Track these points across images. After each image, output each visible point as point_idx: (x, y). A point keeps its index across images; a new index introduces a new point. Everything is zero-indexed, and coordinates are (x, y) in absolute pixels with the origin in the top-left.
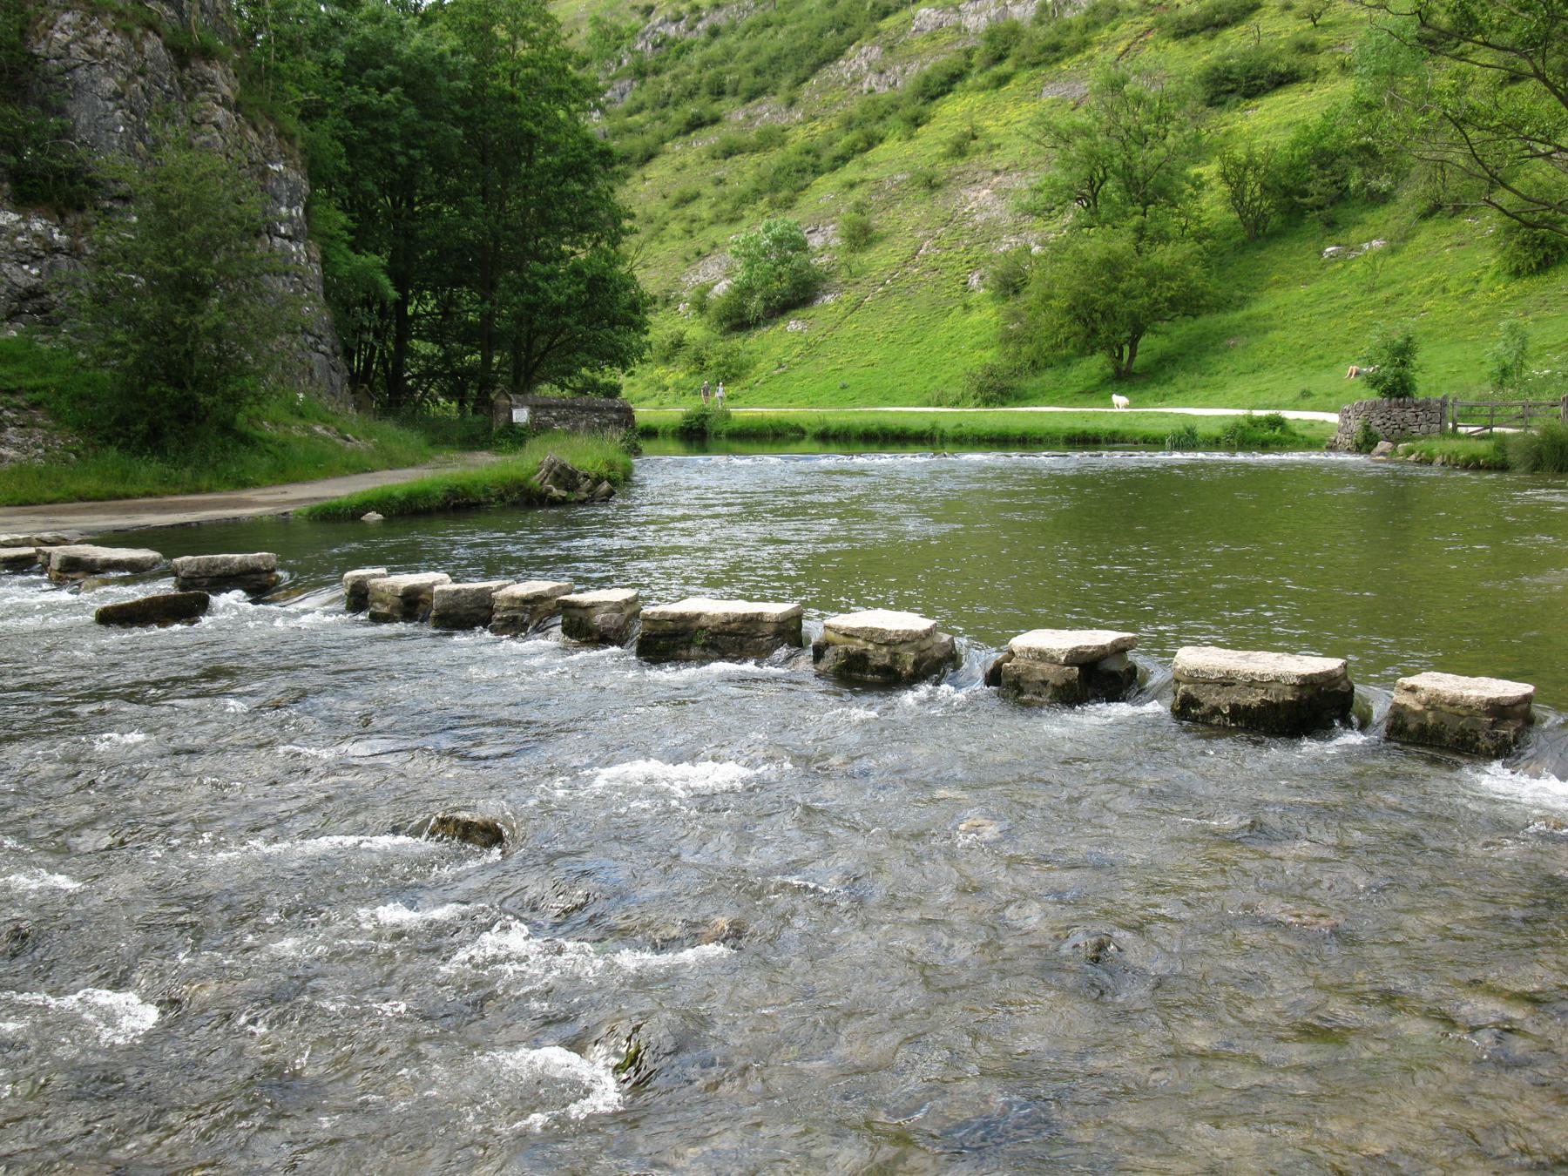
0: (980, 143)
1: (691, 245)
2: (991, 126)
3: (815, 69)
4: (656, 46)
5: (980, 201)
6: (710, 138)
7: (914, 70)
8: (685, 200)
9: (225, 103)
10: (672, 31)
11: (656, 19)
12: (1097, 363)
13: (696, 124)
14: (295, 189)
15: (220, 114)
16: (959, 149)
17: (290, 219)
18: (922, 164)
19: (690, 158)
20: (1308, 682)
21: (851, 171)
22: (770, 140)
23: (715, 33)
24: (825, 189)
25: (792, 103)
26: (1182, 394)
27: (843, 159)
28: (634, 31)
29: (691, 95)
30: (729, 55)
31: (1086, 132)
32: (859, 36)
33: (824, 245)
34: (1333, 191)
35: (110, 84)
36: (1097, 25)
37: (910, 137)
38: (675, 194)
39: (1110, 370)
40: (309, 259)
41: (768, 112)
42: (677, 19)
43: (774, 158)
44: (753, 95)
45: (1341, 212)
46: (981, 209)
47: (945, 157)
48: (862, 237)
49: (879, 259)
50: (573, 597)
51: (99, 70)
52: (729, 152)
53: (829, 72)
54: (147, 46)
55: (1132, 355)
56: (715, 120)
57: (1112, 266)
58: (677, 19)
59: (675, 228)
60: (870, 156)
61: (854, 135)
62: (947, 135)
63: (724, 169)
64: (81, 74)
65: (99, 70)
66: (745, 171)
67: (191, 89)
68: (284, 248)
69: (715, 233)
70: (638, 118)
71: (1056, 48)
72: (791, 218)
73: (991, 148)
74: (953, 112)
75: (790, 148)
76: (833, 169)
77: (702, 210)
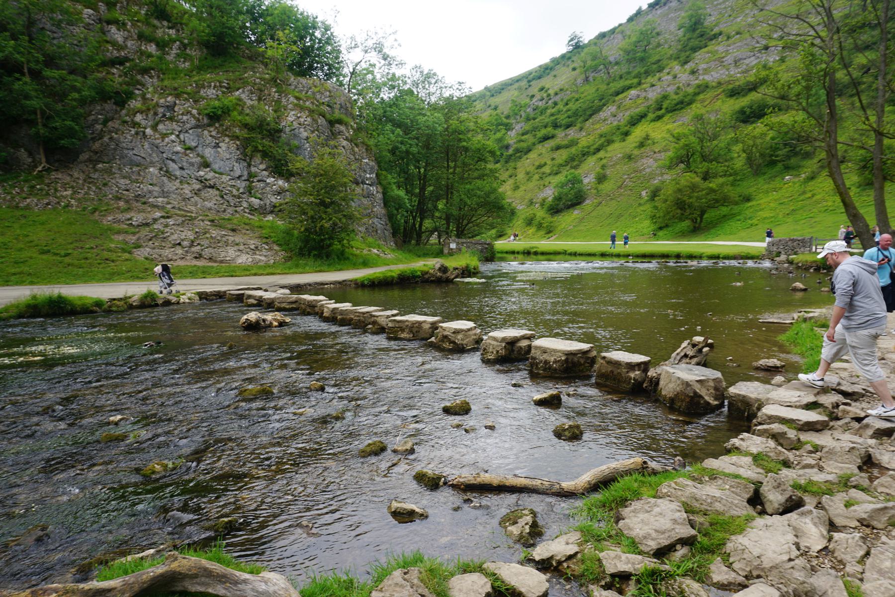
0: (650, 142)
1: (542, 182)
2: (653, 135)
3: (591, 116)
4: (534, 110)
5: (649, 164)
6: (551, 143)
7: (628, 113)
8: (540, 167)
9: (347, 139)
10: (540, 104)
11: (534, 100)
12: (686, 224)
13: (546, 138)
14: (372, 168)
15: (345, 143)
16: (641, 145)
17: (370, 178)
18: (628, 151)
19: (544, 151)
20: (570, 354)
21: (601, 154)
22: (573, 143)
23: (556, 104)
24: (591, 161)
25: (581, 129)
26: (716, 237)
27: (598, 150)
28: (526, 105)
29: (545, 127)
30: (559, 112)
31: (685, 136)
32: (608, 101)
33: (588, 180)
34: (188, 152)
35: (305, 134)
36: (699, 94)
37: (624, 140)
38: (537, 164)
39: (692, 227)
40: (377, 192)
41: (572, 133)
42: (542, 100)
43: (573, 150)
44: (568, 126)
45: (793, 161)
46: (649, 167)
47: (636, 147)
48: (601, 179)
49: (607, 187)
50: (398, 318)
51: (302, 130)
52: (558, 148)
53: (596, 118)
54: (319, 121)
55: (701, 221)
56: (553, 137)
57: (693, 187)
58: (542, 100)
59: (537, 177)
60: (609, 148)
61: (603, 139)
62: (637, 140)
63: (557, 154)
64: (297, 131)
65: (302, 130)
66: (562, 156)
67: (334, 135)
68: (367, 188)
69: (550, 179)
70: (526, 137)
71: (682, 102)
72: (577, 172)
73: (654, 143)
74: (638, 132)
75: (580, 145)
76: (594, 153)
77: (547, 169)
